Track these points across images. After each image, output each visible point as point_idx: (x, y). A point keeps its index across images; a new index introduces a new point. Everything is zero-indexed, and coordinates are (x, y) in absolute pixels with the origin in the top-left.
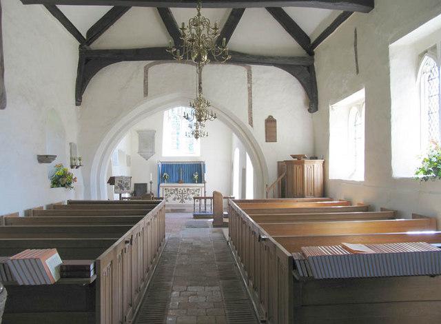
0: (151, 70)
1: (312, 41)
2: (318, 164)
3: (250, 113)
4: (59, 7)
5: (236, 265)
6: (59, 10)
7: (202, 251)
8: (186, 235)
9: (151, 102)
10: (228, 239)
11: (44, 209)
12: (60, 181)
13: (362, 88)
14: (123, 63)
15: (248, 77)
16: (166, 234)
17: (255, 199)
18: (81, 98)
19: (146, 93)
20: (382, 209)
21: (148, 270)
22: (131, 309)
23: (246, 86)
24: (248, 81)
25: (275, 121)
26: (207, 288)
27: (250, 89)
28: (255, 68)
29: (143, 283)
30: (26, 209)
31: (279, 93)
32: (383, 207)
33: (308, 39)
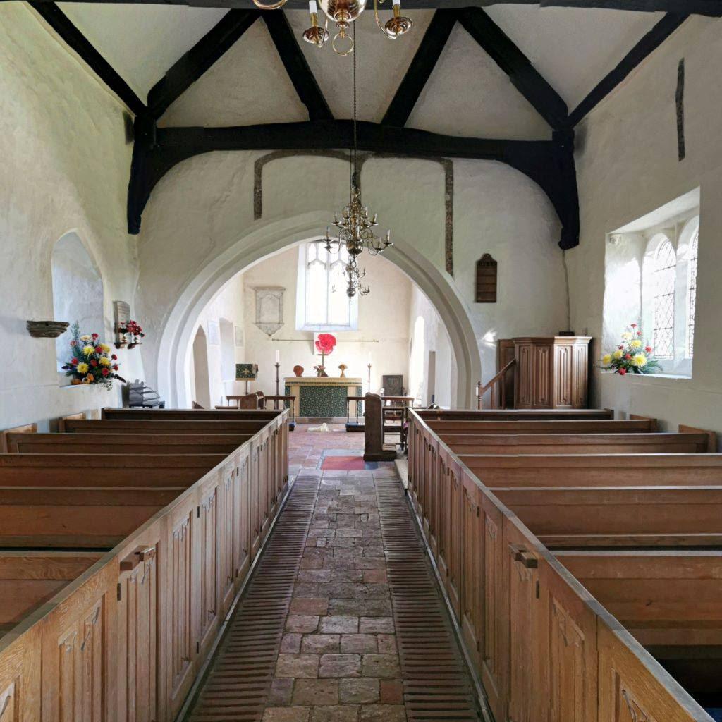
0: (267, 169)
1: (571, 109)
2: (580, 345)
3: (449, 250)
4: (62, 6)
5: (426, 552)
6: (56, 6)
7: (358, 510)
8: (329, 478)
9: (266, 229)
10: (406, 486)
11: (99, 417)
12: (91, 368)
13: (695, 187)
14: (215, 156)
15: (447, 183)
16: (291, 467)
17: (455, 409)
18: (139, 220)
19: (258, 213)
20: (632, 417)
21: (258, 530)
22: (246, 560)
23: (441, 198)
24: (447, 189)
25: (494, 264)
26: (368, 623)
27: (449, 204)
28: (461, 166)
29: (274, 506)
30: (577, 248)
31: (498, 209)
32: (633, 413)
33: (560, 103)
